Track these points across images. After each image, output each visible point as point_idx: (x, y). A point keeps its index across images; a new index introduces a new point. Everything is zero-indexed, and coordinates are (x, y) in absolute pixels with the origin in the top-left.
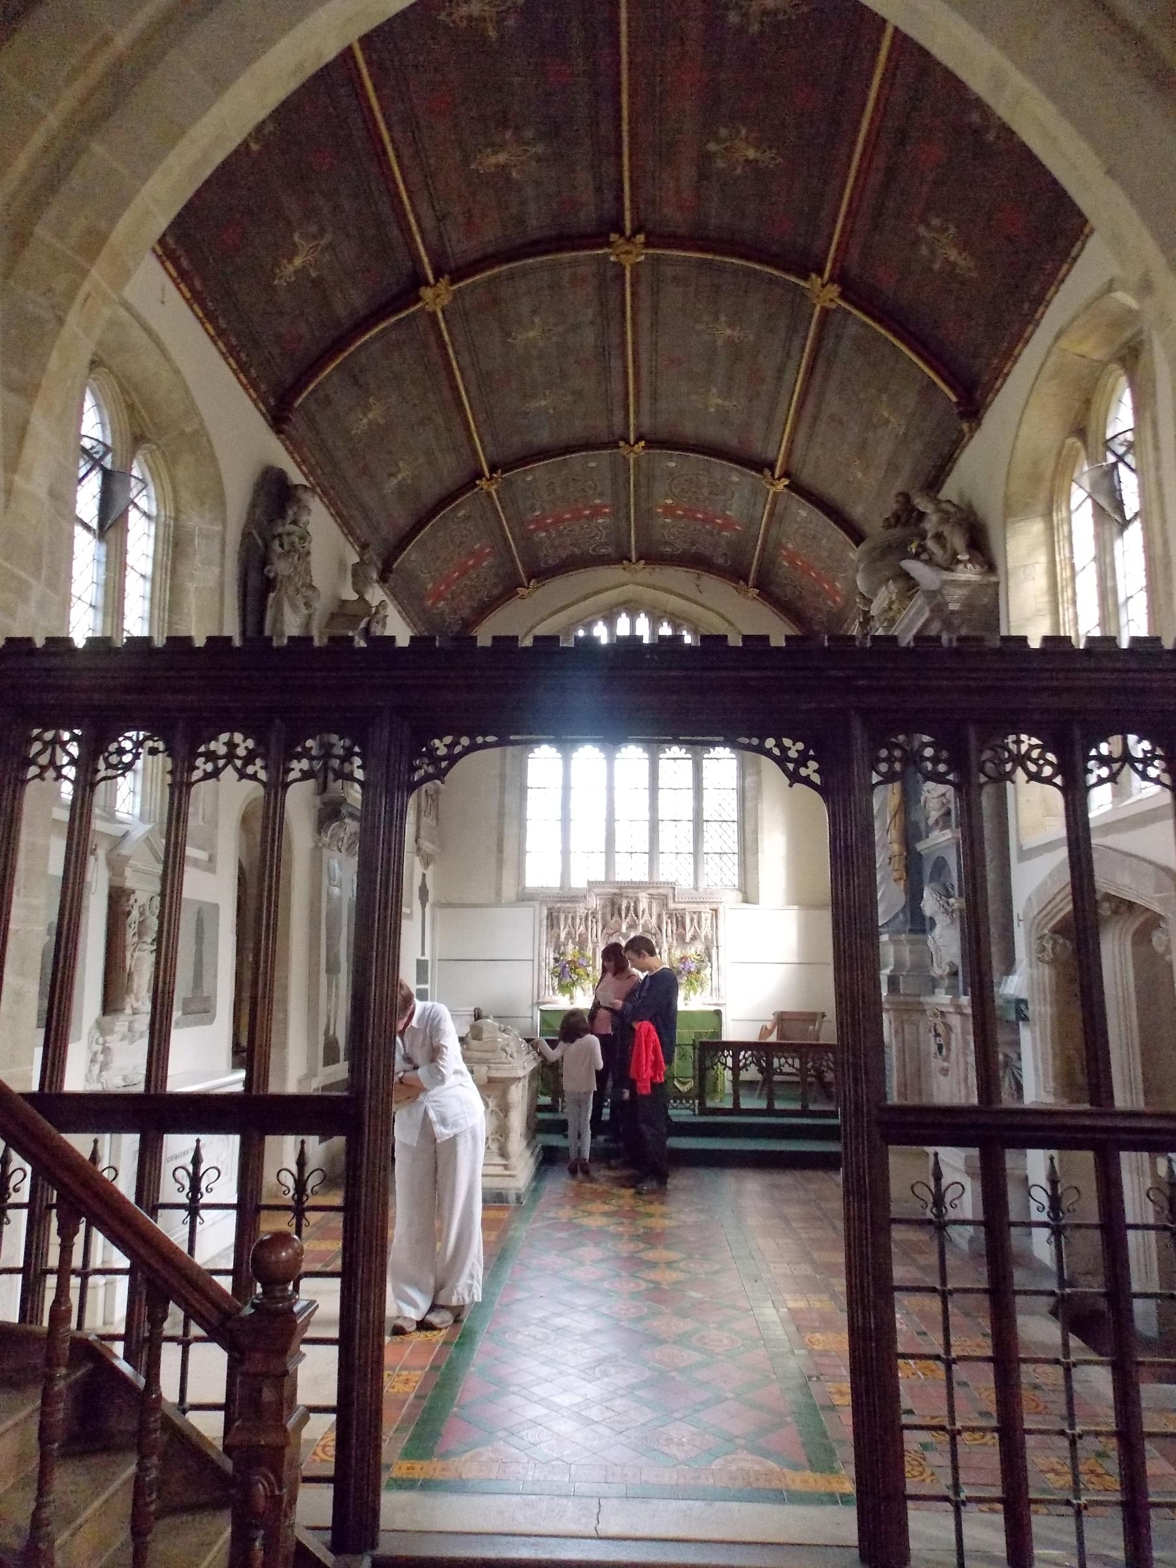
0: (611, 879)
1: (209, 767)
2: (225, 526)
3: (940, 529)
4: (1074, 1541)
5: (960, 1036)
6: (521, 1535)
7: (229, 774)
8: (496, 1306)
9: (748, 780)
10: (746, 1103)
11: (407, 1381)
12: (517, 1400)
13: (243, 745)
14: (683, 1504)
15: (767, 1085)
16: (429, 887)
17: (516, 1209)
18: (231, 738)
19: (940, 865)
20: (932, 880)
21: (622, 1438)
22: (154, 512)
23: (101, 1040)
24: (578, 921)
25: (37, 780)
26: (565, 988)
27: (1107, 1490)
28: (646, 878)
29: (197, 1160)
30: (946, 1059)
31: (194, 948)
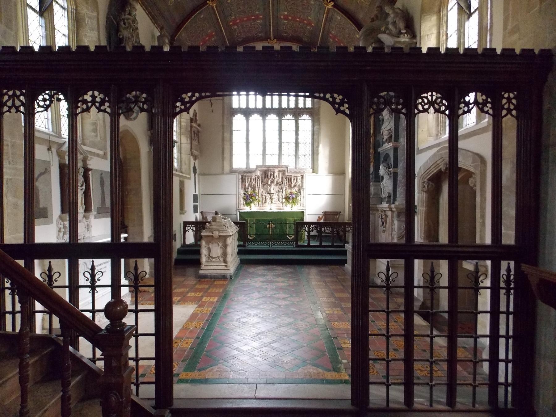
0: (265, 165)
1: (85, 106)
2: (98, 14)
3: (395, 20)
4: (429, 396)
5: (390, 219)
6: (226, 399)
7: (94, 110)
8: (221, 315)
9: (316, 127)
10: (312, 243)
11: (187, 343)
12: (228, 349)
13: (99, 97)
14: (287, 385)
15: (320, 237)
16: (197, 168)
17: (230, 280)
18: (93, 93)
19: (387, 156)
20: (383, 162)
21: (265, 362)
22: (66, 6)
23: (62, 223)
24: (252, 180)
25: (8, 113)
26: (248, 204)
27: (438, 376)
28: (277, 164)
29: (93, 268)
30: (385, 227)
31: (100, 188)
